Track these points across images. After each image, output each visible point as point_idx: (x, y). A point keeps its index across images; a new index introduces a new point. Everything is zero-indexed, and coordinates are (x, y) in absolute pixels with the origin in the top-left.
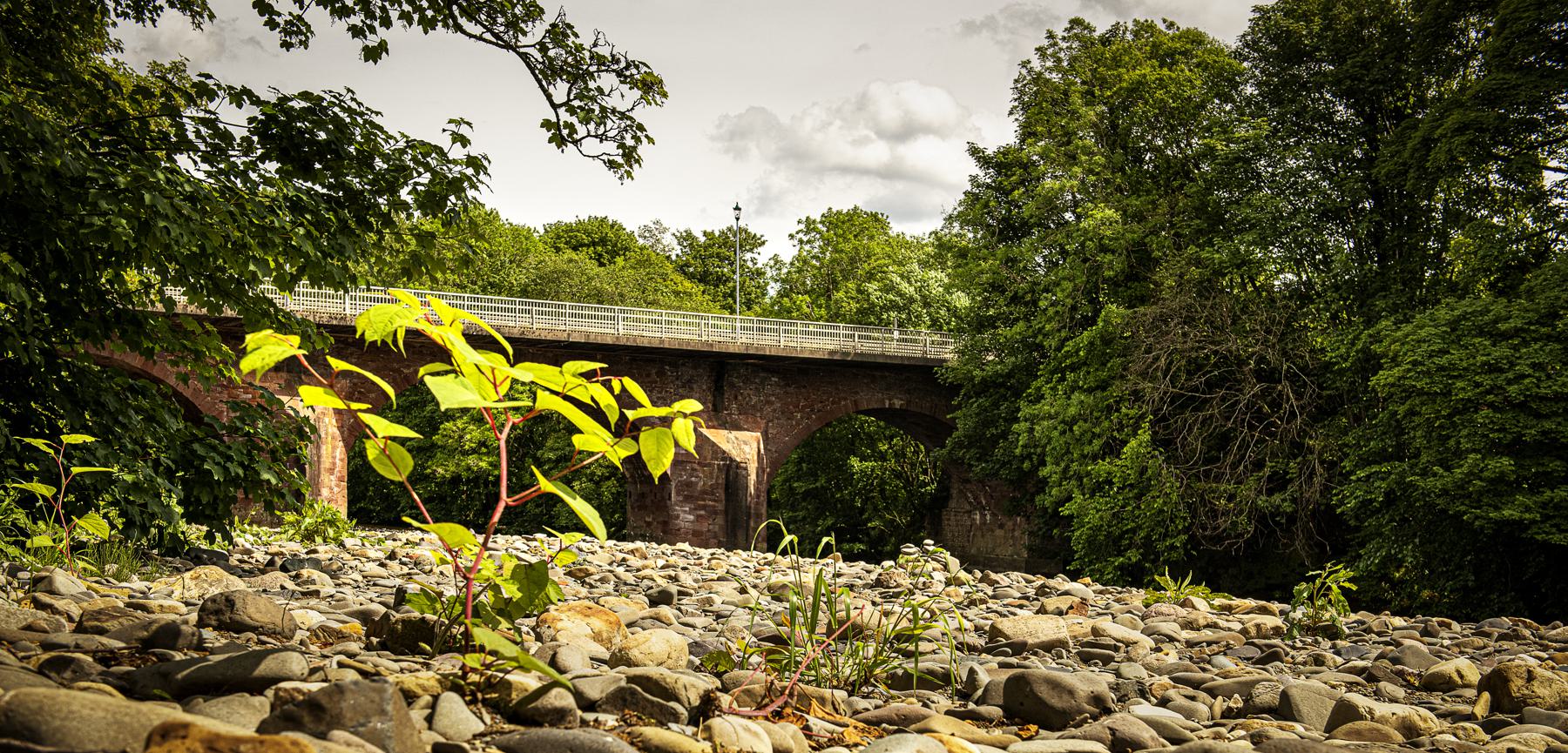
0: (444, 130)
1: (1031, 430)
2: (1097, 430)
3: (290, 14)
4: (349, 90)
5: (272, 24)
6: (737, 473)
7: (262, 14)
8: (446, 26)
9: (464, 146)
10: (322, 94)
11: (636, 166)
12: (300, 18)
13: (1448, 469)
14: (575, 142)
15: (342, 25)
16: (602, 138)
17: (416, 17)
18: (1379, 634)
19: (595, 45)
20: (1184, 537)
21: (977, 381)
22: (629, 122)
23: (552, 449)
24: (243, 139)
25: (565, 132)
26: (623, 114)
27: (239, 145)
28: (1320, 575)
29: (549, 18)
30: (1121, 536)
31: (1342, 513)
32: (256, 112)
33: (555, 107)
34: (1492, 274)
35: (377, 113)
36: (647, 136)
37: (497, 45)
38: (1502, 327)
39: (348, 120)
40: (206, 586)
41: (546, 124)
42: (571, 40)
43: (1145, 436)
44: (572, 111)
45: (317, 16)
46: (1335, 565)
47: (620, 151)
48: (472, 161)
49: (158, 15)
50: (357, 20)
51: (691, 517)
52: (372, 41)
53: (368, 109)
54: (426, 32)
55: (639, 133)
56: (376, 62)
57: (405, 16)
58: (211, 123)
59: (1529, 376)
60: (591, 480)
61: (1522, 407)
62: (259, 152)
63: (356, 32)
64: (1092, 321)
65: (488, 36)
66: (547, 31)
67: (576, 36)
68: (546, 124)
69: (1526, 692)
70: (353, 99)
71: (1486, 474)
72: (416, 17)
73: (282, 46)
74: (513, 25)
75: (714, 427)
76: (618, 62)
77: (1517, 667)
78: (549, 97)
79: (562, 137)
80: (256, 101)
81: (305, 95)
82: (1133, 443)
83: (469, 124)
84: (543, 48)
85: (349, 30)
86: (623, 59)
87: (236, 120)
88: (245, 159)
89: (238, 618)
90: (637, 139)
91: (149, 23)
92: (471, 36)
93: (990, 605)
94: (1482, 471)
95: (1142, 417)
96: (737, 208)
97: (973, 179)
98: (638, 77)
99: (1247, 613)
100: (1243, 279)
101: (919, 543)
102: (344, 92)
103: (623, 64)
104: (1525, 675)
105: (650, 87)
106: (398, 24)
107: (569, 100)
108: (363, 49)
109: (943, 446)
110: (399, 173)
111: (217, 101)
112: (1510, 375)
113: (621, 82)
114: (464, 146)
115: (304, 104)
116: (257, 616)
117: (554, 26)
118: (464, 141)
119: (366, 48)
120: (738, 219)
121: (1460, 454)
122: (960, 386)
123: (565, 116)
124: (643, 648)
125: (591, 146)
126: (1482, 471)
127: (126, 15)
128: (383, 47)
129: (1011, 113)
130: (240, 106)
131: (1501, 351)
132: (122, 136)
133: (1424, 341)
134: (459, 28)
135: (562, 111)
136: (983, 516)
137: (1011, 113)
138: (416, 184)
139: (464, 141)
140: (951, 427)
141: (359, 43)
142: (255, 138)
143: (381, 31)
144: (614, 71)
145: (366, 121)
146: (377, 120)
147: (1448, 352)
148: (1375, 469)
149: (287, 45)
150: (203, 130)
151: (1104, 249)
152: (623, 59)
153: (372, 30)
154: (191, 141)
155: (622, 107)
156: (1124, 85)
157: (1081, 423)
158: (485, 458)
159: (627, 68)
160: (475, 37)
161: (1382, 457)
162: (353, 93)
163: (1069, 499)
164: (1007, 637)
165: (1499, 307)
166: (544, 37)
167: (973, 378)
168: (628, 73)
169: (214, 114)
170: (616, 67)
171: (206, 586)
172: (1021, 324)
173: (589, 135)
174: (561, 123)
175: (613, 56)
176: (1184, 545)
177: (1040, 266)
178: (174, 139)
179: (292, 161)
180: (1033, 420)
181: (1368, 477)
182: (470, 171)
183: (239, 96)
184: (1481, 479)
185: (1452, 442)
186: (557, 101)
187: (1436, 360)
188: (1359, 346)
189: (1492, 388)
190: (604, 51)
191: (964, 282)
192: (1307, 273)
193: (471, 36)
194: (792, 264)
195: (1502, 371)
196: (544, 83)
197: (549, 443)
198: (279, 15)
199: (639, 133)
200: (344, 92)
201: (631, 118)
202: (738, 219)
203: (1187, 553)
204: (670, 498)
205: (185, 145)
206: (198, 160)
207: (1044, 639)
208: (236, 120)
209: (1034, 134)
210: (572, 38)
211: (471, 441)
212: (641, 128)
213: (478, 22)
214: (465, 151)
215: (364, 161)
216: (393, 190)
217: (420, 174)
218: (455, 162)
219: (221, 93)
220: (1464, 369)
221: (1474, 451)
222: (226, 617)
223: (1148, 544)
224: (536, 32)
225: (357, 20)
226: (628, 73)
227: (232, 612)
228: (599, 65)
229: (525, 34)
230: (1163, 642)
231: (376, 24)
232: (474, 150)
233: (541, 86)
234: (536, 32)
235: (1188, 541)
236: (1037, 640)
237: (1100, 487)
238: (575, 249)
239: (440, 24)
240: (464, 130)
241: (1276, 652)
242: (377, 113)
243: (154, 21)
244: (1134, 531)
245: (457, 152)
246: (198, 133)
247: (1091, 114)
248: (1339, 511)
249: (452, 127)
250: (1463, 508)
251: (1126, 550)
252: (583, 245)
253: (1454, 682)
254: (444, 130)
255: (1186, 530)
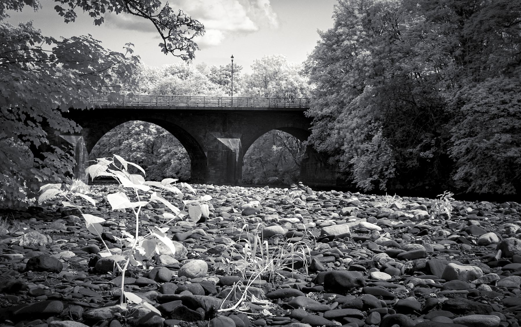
0: (124, 48)
1: (339, 133)
2: (363, 132)
3: (68, 10)
4: (90, 35)
5: (62, 14)
6: (231, 154)
7: (57, 11)
8: (125, 11)
9: (131, 53)
10: (80, 37)
11: (193, 59)
12: (72, 11)
13: (489, 140)
14: (171, 51)
15: (87, 13)
16: (181, 49)
17: (114, 8)
18: (463, 216)
19: (179, 15)
20: (394, 169)
21: (320, 115)
22: (191, 43)
23: (163, 148)
24: (51, 55)
25: (168, 48)
26: (189, 40)
27: (49, 58)
28: (442, 196)
29: (163, 6)
30: (371, 171)
31: (451, 157)
32: (55, 46)
33: (164, 38)
34: (503, 68)
35: (100, 42)
36: (197, 47)
37: (143, 16)
38: (507, 87)
39: (89, 45)
40: (32, 239)
41: (161, 45)
42: (171, 14)
43: (380, 134)
44: (170, 40)
45: (78, 10)
46: (447, 192)
47: (188, 54)
48: (135, 58)
49: (22, 7)
50: (92, 10)
51: (214, 171)
52: (98, 17)
53: (96, 40)
54: (117, 14)
55: (195, 46)
56: (99, 25)
57: (110, 8)
58: (38, 50)
59: (516, 105)
60: (178, 159)
61: (514, 115)
62: (57, 60)
63: (92, 14)
64: (361, 91)
65: (140, 14)
66: (162, 11)
67: (173, 12)
68: (161, 45)
69: (514, 249)
70: (91, 38)
71: (501, 141)
72: (114, 8)
73: (65, 22)
74: (149, 9)
75: (223, 138)
76: (188, 20)
77: (511, 240)
78: (162, 35)
79: (167, 50)
80: (55, 42)
81: (74, 38)
82: (376, 136)
83: (133, 45)
84: (160, 17)
85: (90, 14)
86: (189, 19)
87: (48, 49)
88: (51, 63)
89: (41, 266)
90: (194, 49)
91: (19, 10)
92: (134, 14)
93: (322, 211)
94: (500, 140)
95: (379, 126)
96: (232, 57)
97: (319, 42)
98: (195, 25)
99: (416, 209)
100: (415, 74)
101: (298, 184)
102: (88, 36)
103: (189, 21)
104: (514, 243)
105: (199, 29)
106: (107, 11)
107: (169, 36)
108: (95, 21)
109: (307, 140)
110: (109, 64)
111: (41, 43)
112: (510, 105)
113: (189, 28)
114: (131, 53)
115: (73, 41)
116: (48, 265)
117: (164, 8)
118: (131, 51)
119: (96, 21)
120: (232, 61)
121: (493, 134)
122: (313, 118)
123: (167, 42)
124: (191, 268)
125: (177, 52)
126: (500, 140)
127: (11, 8)
128: (102, 20)
129: (333, 17)
130: (50, 44)
131: (506, 97)
132: (7, 58)
133: (480, 94)
134: (130, 12)
135: (167, 40)
136: (321, 165)
137: (333, 17)
138: (113, 68)
139: (131, 51)
140: (310, 133)
141: (93, 19)
142: (55, 55)
143: (102, 15)
144: (186, 24)
145: (96, 45)
146: (99, 44)
147: (488, 97)
148: (463, 140)
149: (67, 21)
150: (37, 54)
151: (365, 65)
152: (189, 19)
153: (98, 14)
154: (32, 58)
155: (188, 37)
156: (374, 5)
157: (357, 130)
158: (139, 153)
159: (191, 23)
160: (135, 14)
161: (465, 136)
162: (91, 36)
163: (353, 157)
164: (327, 234)
165: (507, 80)
166: (161, 13)
167: (318, 114)
168: (191, 24)
169: (40, 48)
170: (187, 22)
171: (32, 239)
172: (335, 94)
173: (176, 48)
174: (167, 44)
175: (185, 18)
176: (395, 172)
177: (342, 72)
178: (26, 58)
179: (68, 62)
180: (340, 129)
181: (460, 144)
182: (133, 62)
183: (49, 40)
184: (499, 143)
185: (490, 130)
186: (165, 36)
187: (484, 100)
188: (456, 96)
189: (504, 110)
190: (182, 17)
191: (314, 79)
192: (438, 70)
193: (134, 14)
194: (252, 76)
195: (506, 103)
196: (161, 29)
197: (163, 146)
198: (64, 10)
199: (195, 46)
200: (88, 36)
201: (192, 42)
202: (232, 61)
203: (396, 174)
204: (207, 165)
205: (29, 59)
206: (35, 64)
207: (341, 233)
208: (48, 49)
209: (341, 24)
210: (171, 12)
211: (134, 147)
212: (195, 44)
213: (136, 9)
214: (131, 55)
215: (94, 61)
216: (105, 70)
217: (115, 64)
218: (127, 59)
219: (43, 40)
220: (494, 103)
221: (498, 133)
222: (37, 266)
223: (381, 172)
224: (158, 11)
225: (92, 10)
226: (191, 24)
227: (39, 264)
228: (180, 22)
229: (153, 12)
230: (385, 228)
231: (100, 12)
232: (134, 54)
233: (159, 31)
234: (158, 11)
235: (396, 170)
236: (338, 234)
237: (364, 152)
238: (173, 74)
239: (123, 10)
240: (131, 47)
241: (426, 231)
242: (100, 42)
243: (21, 9)
244: (376, 168)
245: (128, 55)
246: (34, 55)
247: (360, 16)
248: (450, 157)
249: (127, 46)
250: (493, 153)
251: (373, 175)
252: (175, 73)
253: (489, 242)
254: (124, 48)
255: (395, 167)
